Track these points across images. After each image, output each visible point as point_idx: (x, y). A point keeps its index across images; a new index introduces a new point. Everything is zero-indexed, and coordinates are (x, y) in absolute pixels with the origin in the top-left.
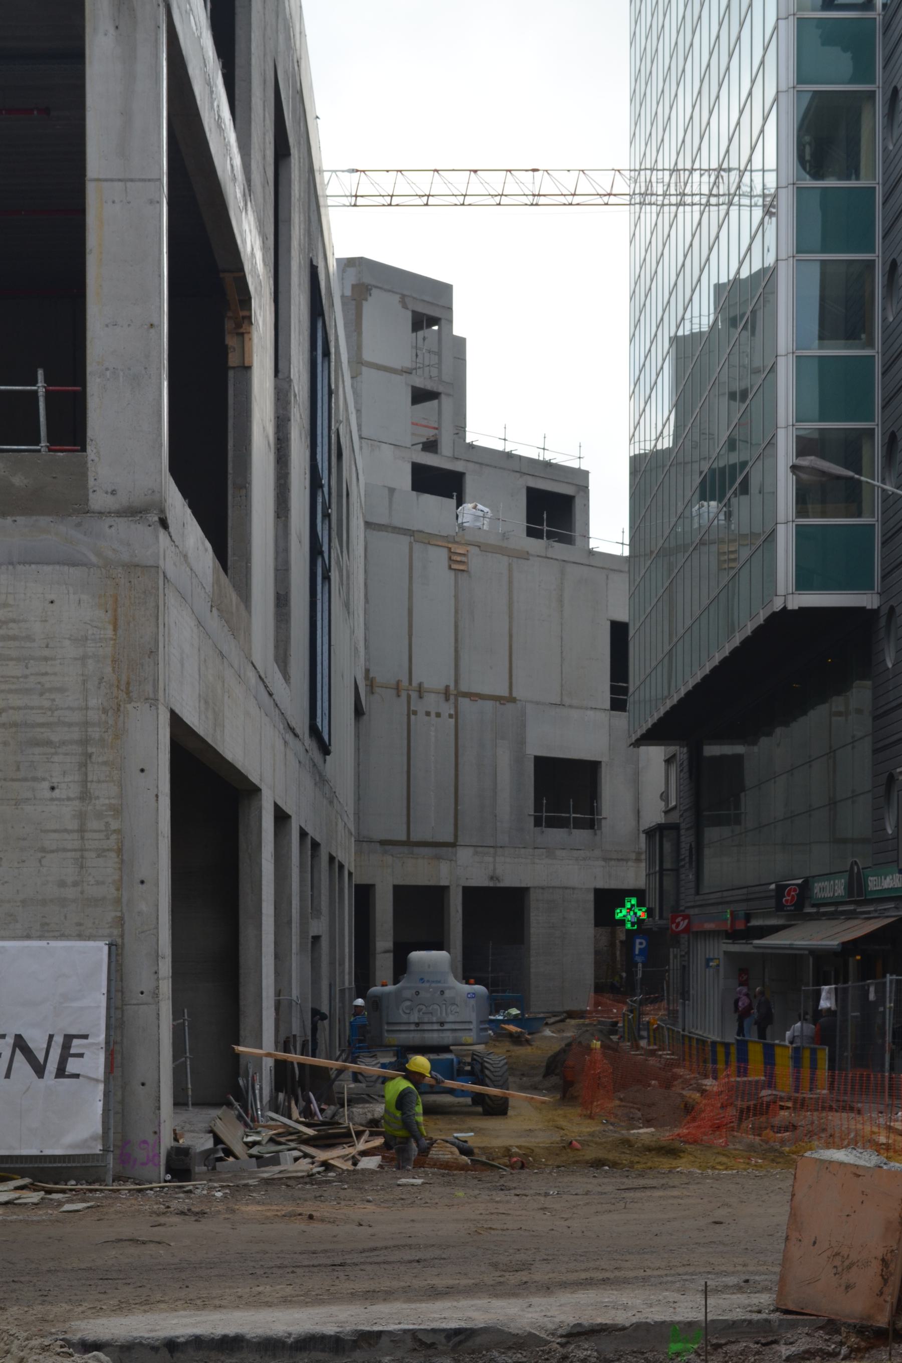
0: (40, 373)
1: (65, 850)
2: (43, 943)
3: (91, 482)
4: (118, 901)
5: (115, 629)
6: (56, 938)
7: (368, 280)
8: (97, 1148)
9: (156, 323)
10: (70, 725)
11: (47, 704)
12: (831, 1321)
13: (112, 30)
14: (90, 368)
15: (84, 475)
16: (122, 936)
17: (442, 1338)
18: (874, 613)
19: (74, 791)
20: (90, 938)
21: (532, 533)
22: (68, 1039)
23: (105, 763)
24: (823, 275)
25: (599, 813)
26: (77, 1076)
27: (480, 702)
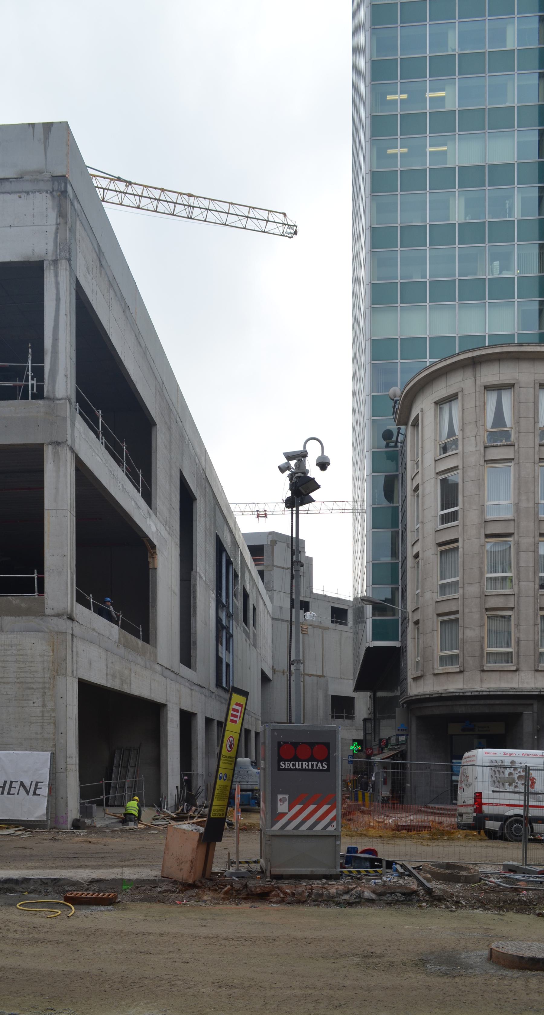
0: (35, 571)
1: (37, 723)
2: (30, 752)
3: (46, 606)
4: (54, 739)
5: (53, 652)
6: (35, 751)
7: (276, 539)
8: (45, 818)
9: (66, 554)
10: (39, 683)
11: (32, 676)
12: (175, 881)
13: (52, 462)
14: (45, 570)
15: (44, 603)
16: (55, 750)
17: (50, 881)
18: (399, 648)
19: (40, 704)
20: (45, 751)
21: (332, 622)
22: (37, 783)
23: (50, 695)
24: (392, 535)
25: (354, 714)
26: (39, 795)
27: (312, 677)
